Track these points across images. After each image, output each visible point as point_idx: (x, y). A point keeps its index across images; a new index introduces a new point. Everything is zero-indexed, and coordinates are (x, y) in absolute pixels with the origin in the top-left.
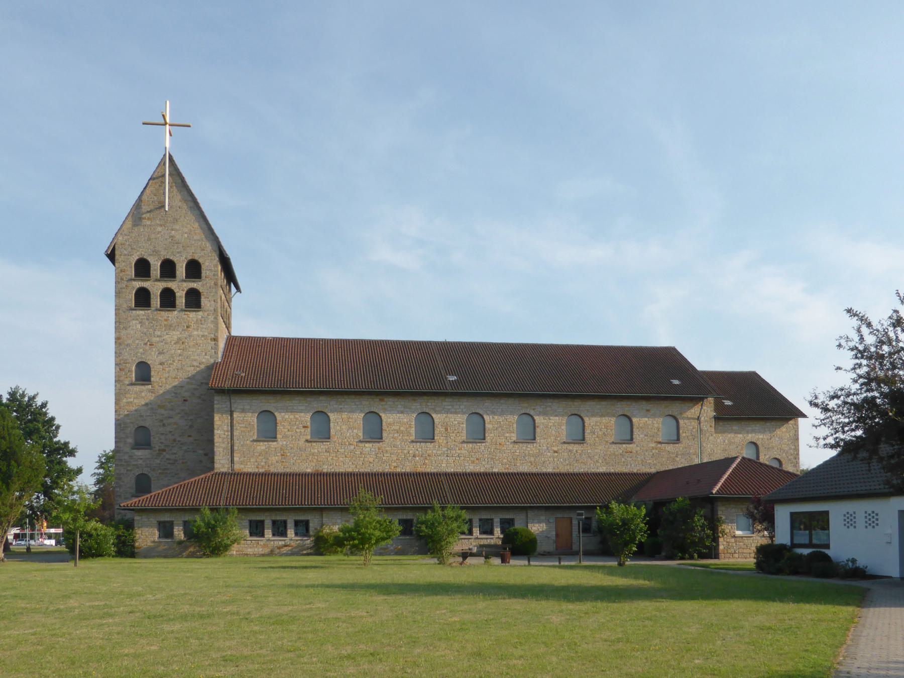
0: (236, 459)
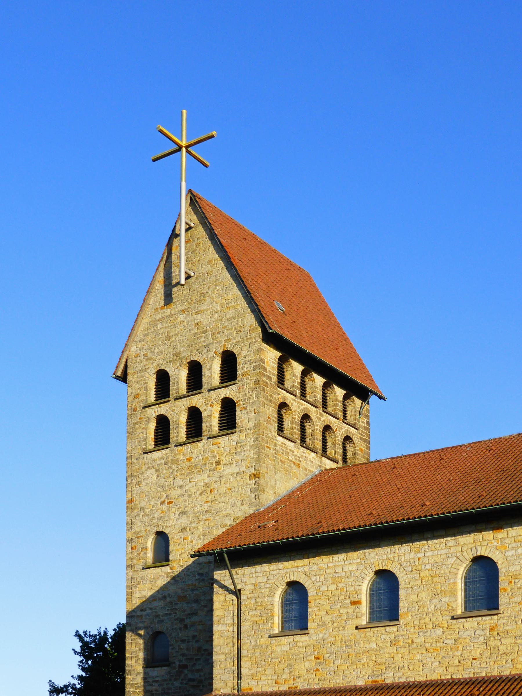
0: (244, 671)
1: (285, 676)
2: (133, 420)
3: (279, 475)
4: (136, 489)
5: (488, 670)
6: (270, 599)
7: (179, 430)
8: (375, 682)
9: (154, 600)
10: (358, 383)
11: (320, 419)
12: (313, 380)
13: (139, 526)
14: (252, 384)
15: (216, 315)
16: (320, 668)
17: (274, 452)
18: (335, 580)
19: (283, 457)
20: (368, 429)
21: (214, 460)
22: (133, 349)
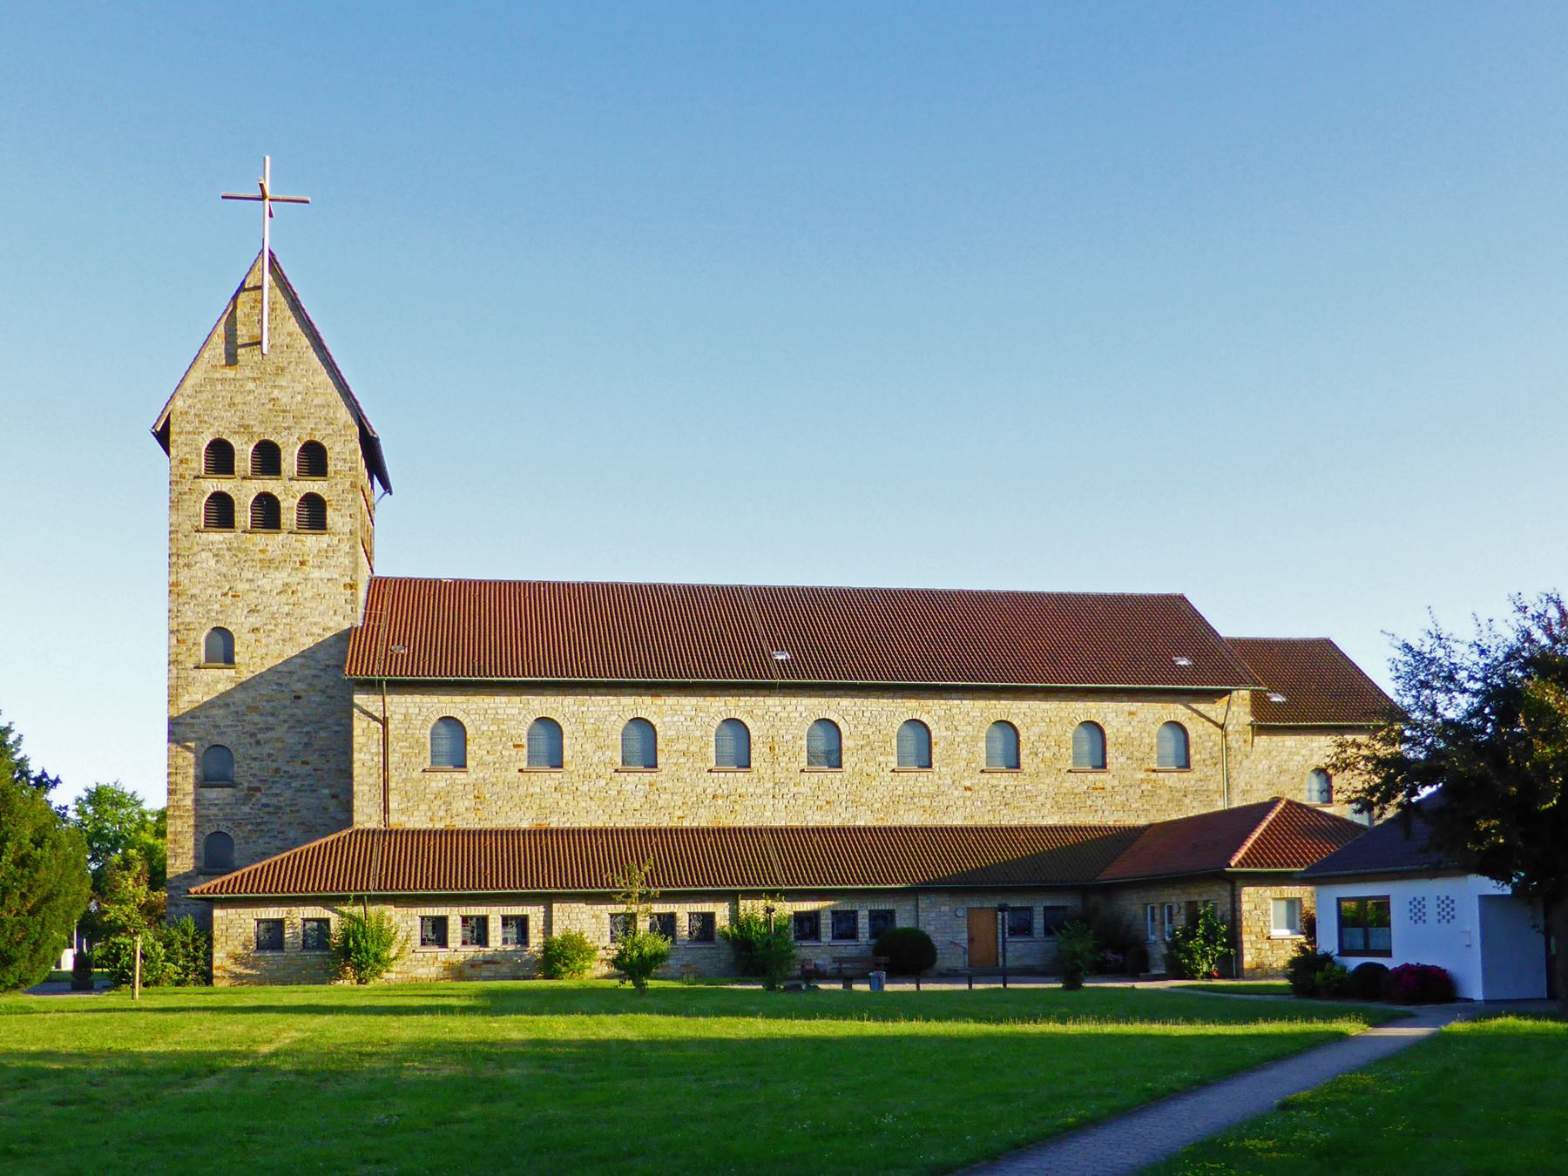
1: (442, 813)
2: (179, 488)
13: (189, 614)
14: (347, 485)
15: (299, 398)
18: (495, 721)
22: (179, 403)
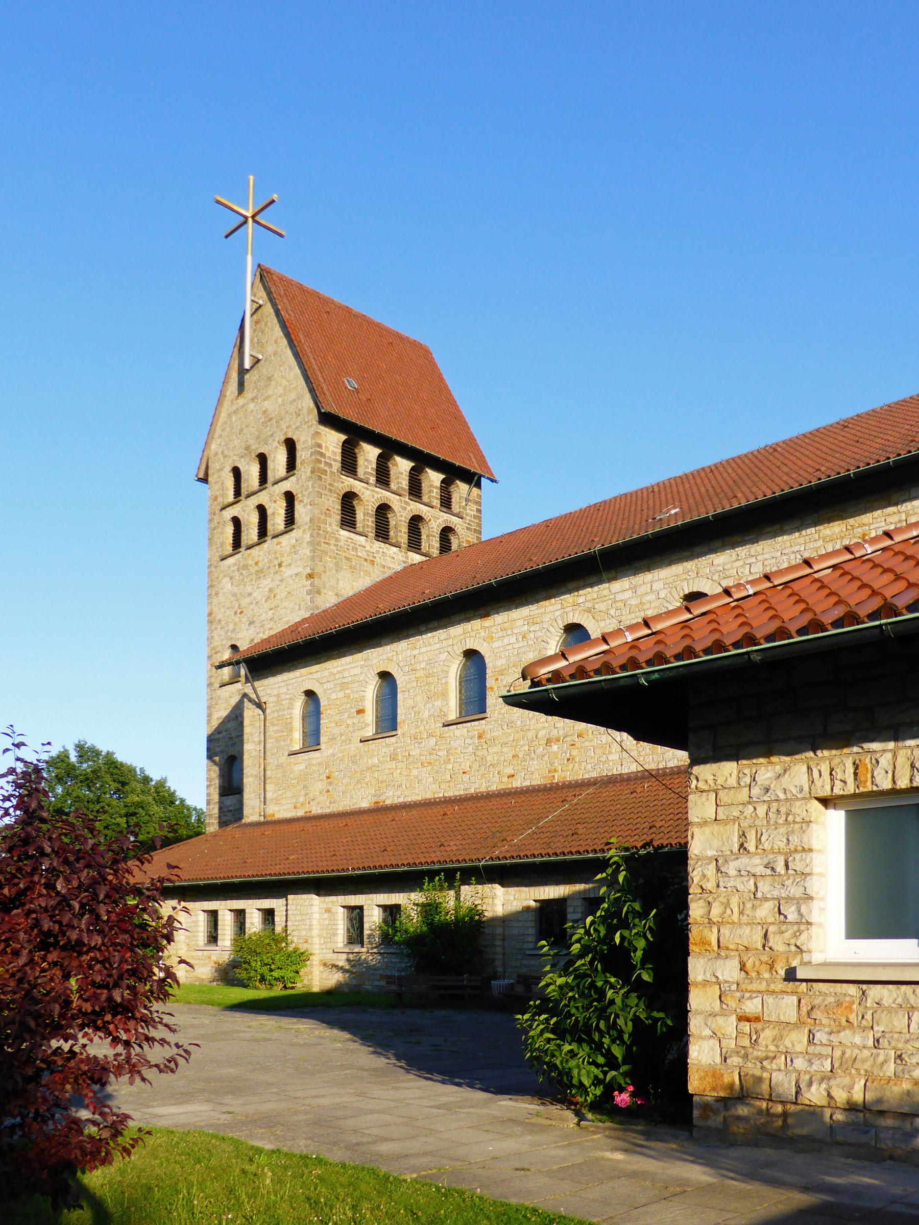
1: (302, 799)
3: (343, 573)
4: (215, 600)
5: (477, 785)
6: (289, 711)
7: (251, 533)
8: (377, 803)
9: (229, 721)
10: (454, 465)
11: (405, 509)
12: (396, 465)
15: (280, 400)
16: (330, 788)
17: (335, 548)
18: (344, 686)
19: (349, 554)
20: (480, 518)
21: (276, 563)
22: (213, 447)
